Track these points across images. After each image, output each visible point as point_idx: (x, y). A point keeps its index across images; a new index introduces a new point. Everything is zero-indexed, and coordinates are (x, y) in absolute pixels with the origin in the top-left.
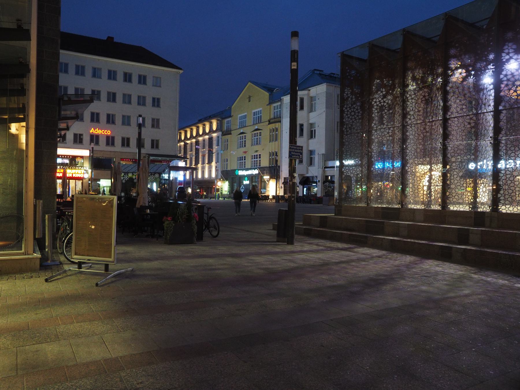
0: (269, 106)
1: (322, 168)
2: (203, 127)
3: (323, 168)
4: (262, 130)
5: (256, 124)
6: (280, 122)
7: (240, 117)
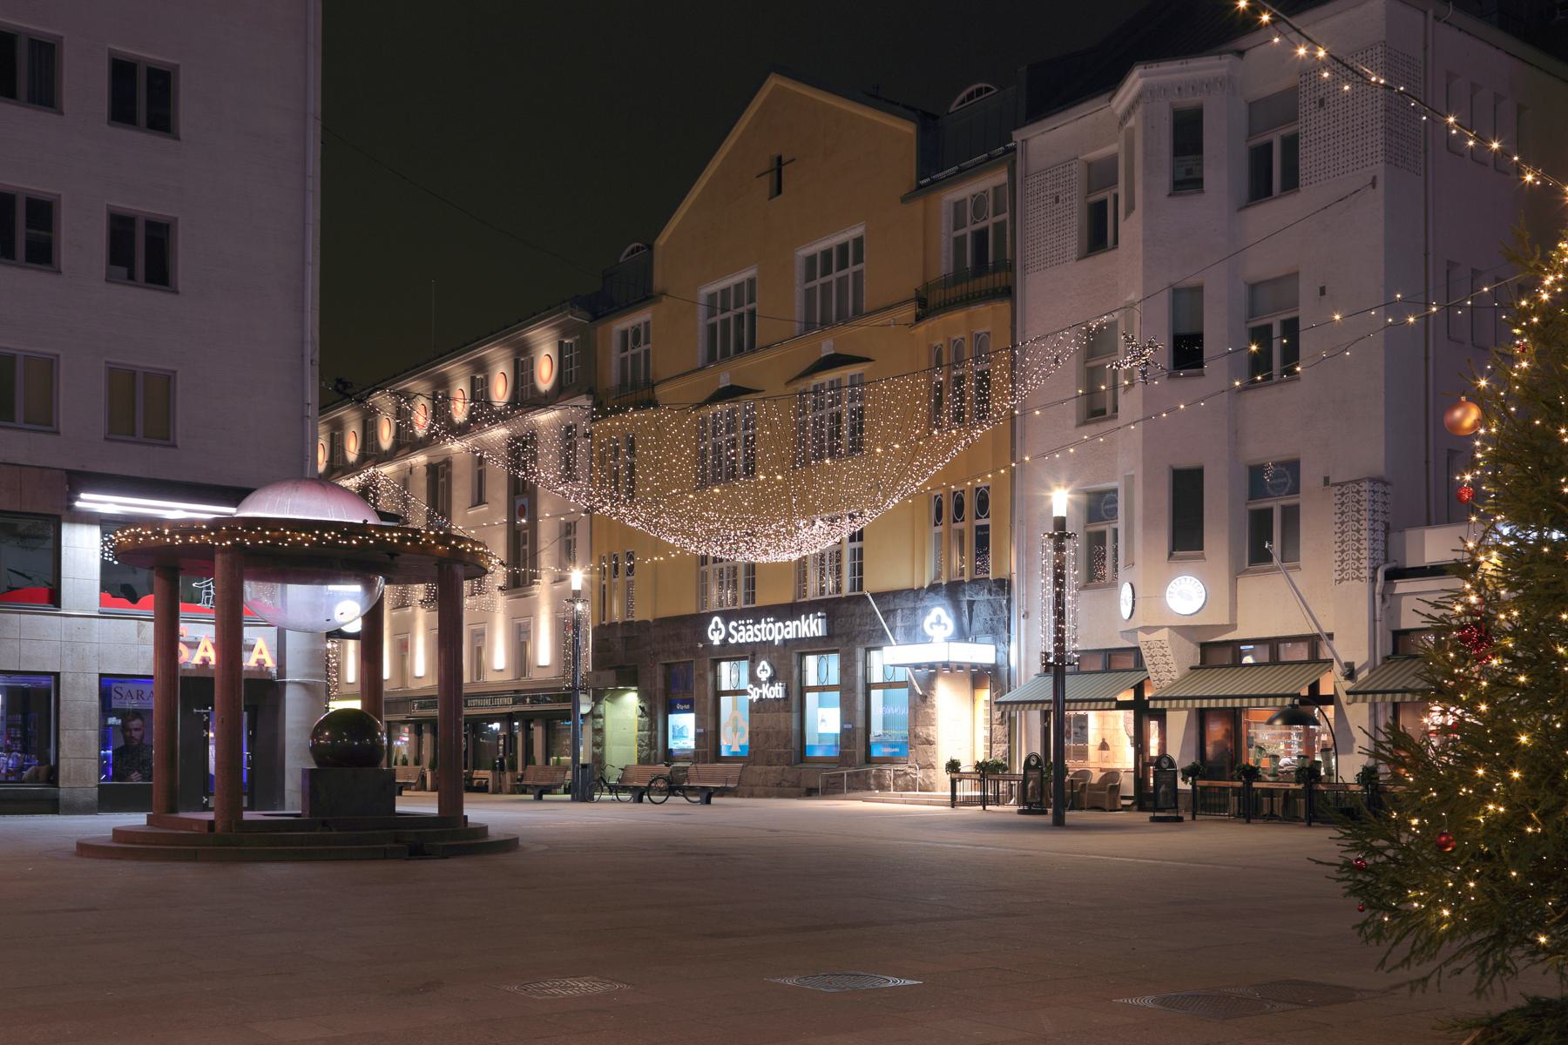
0: (918, 206)
1: (1374, 579)
2: (473, 379)
3: (1380, 575)
4: (868, 360)
5: (825, 322)
6: (1007, 292)
7: (712, 296)
